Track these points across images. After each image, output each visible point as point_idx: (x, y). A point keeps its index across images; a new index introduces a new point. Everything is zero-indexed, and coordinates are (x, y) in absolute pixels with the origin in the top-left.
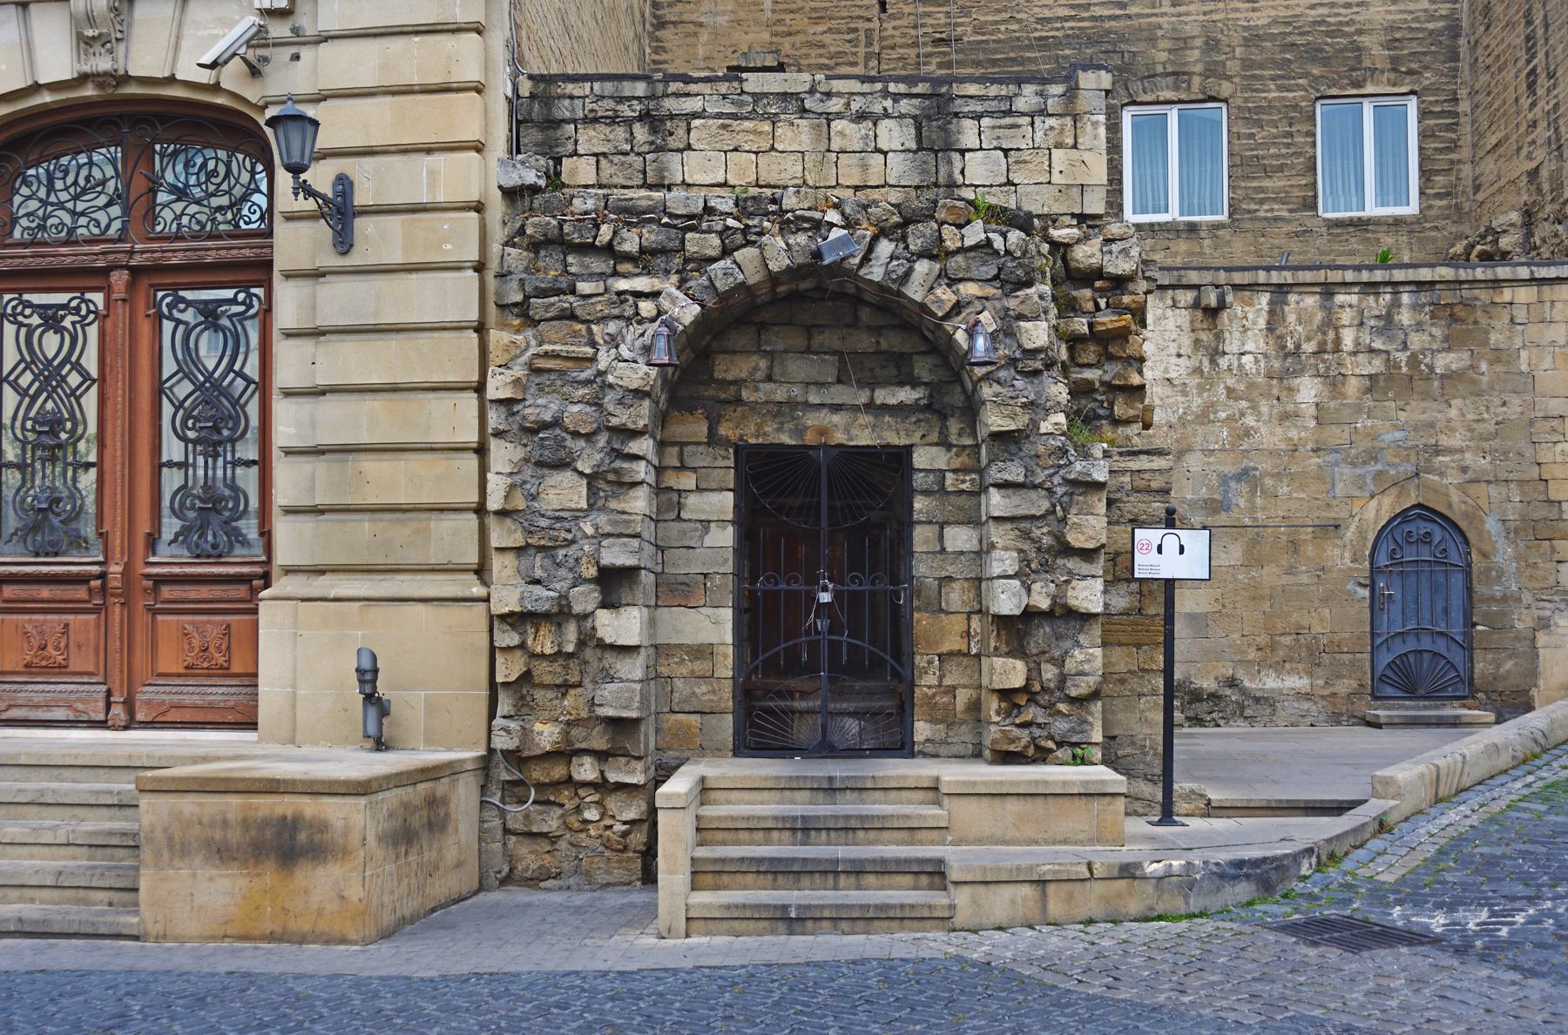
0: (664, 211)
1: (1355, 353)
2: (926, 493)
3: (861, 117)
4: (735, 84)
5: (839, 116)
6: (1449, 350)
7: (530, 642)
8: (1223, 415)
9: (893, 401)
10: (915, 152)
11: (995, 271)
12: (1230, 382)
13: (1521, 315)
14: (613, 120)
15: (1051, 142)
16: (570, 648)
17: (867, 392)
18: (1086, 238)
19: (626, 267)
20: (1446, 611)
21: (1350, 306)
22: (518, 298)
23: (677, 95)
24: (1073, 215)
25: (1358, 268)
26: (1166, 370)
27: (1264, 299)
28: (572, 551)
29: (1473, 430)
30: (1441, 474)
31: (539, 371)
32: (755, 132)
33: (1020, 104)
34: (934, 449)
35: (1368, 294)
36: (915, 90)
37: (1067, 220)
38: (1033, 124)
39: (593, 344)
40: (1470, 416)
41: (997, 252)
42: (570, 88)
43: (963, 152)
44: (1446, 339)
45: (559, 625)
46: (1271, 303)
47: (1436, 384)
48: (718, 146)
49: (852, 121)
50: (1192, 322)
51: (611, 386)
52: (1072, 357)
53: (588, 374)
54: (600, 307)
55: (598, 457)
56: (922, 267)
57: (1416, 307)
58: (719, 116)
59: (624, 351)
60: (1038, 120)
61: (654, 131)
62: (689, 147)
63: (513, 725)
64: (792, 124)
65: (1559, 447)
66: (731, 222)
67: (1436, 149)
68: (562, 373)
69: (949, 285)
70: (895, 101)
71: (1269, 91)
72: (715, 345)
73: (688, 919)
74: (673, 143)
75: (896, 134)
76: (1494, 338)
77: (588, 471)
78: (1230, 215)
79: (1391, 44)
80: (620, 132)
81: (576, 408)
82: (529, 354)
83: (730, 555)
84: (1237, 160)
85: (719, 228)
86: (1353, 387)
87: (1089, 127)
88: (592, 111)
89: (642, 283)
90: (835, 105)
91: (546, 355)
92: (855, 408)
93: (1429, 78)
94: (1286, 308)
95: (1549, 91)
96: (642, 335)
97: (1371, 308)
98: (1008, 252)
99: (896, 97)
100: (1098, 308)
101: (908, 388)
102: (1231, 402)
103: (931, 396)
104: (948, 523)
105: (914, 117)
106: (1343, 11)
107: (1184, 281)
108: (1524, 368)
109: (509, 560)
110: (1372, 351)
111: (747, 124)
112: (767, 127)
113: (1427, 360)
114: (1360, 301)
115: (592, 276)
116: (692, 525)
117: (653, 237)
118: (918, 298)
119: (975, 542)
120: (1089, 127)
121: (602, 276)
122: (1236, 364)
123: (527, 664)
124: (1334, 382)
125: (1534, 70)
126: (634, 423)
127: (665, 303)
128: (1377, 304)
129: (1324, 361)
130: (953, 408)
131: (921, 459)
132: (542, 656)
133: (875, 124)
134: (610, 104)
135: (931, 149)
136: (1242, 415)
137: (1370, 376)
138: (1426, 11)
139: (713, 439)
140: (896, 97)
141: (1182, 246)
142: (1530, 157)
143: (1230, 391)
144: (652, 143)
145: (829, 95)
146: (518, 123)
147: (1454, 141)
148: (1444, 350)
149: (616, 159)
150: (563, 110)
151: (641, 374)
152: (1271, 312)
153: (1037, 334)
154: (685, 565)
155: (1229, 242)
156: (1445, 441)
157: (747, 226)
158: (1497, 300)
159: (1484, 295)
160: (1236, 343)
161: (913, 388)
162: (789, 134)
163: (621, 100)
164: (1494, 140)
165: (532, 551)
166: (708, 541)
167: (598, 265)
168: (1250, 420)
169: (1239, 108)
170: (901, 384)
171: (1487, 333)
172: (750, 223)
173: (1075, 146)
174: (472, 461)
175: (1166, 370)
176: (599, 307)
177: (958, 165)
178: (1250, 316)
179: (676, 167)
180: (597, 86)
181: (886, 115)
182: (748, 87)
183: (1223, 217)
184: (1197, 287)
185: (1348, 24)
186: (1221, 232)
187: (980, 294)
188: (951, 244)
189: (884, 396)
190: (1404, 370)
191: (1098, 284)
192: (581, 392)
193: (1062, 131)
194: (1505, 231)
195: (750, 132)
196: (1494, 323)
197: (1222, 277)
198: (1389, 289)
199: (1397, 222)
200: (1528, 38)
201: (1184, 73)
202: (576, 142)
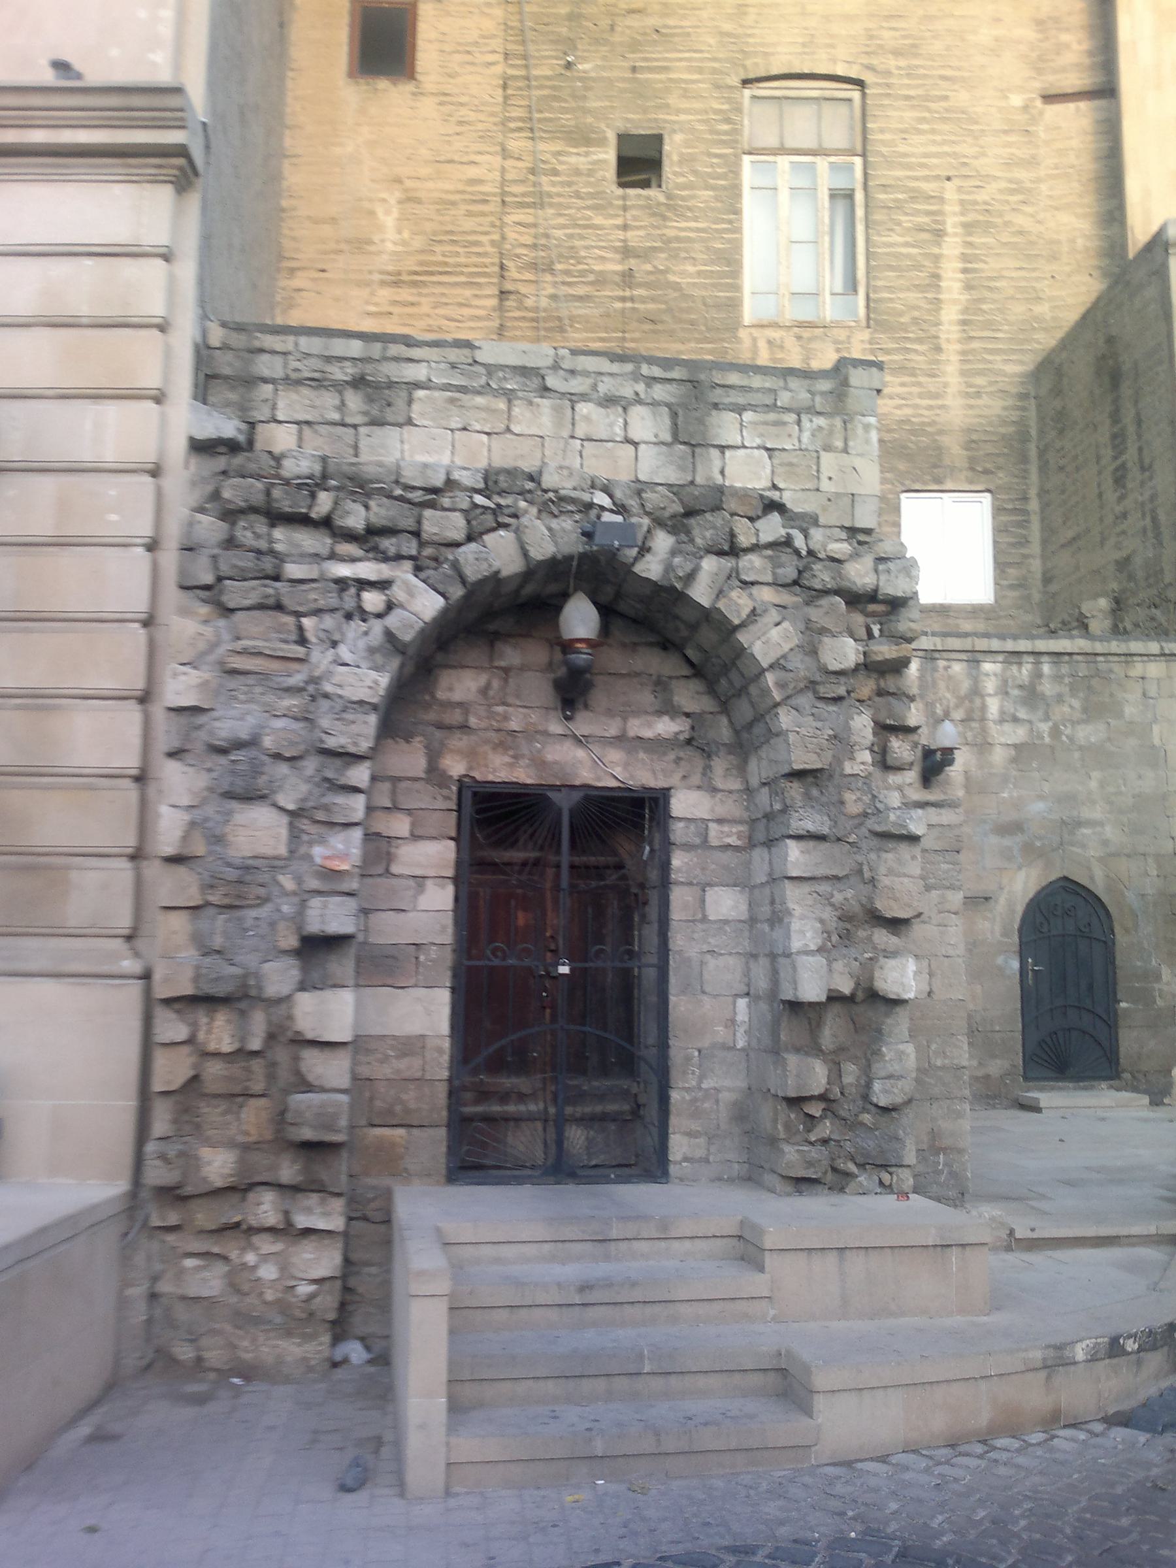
2: (688, 847)
3: (609, 401)
4: (466, 351)
5: (584, 397)
6: (1086, 721)
7: (201, 1036)
9: (648, 733)
11: (794, 575)
13: (1153, 691)
14: (318, 383)
15: (818, 445)
16: (255, 1044)
18: (856, 555)
20: (1090, 987)
22: (209, 579)
23: (396, 359)
24: (842, 527)
25: (1002, 637)
28: (264, 912)
29: (1111, 803)
30: (1084, 846)
31: (234, 672)
32: (487, 409)
35: (1011, 663)
36: (669, 375)
38: (799, 423)
39: (302, 641)
40: (1111, 789)
41: (797, 552)
42: (269, 341)
43: (722, 448)
44: (1085, 710)
45: (243, 1013)
47: (1077, 755)
48: (444, 423)
49: (600, 405)
51: (326, 696)
53: (297, 680)
54: (315, 596)
55: (304, 788)
56: (709, 564)
57: (1057, 678)
58: (447, 387)
59: (344, 652)
60: (804, 418)
61: (370, 400)
62: (410, 422)
63: (172, 1150)
64: (531, 403)
66: (479, 499)
68: (263, 676)
70: (648, 386)
73: (449, 1464)
77: (291, 807)
79: (969, 445)
80: (329, 399)
81: (280, 723)
82: (221, 650)
85: (465, 505)
86: (999, 756)
87: (860, 431)
88: (297, 370)
89: (368, 570)
90: (577, 385)
91: (245, 652)
95: (1142, 483)
97: (1014, 678)
98: (811, 553)
99: (651, 381)
100: (870, 635)
101: (666, 718)
104: (710, 885)
105: (668, 405)
106: (926, 413)
109: (179, 923)
111: (480, 400)
112: (502, 405)
113: (1068, 731)
114: (1004, 670)
116: (404, 882)
117: (383, 512)
118: (705, 602)
119: (744, 907)
121: (317, 557)
123: (195, 1066)
125: (1123, 467)
126: (355, 744)
127: (398, 593)
131: (686, 804)
132: (217, 1055)
133: (625, 409)
137: (1015, 746)
138: (999, 416)
139: (435, 775)
140: (651, 381)
142: (1118, 547)
149: (323, 429)
150: (266, 366)
154: (392, 930)
156: (1086, 813)
157: (499, 506)
159: (1118, 669)
161: (672, 719)
162: (528, 415)
163: (329, 359)
164: (1070, 534)
165: (211, 911)
167: (310, 541)
170: (660, 713)
172: (503, 502)
173: (845, 450)
174: (131, 793)
176: (313, 596)
177: (717, 464)
181: (639, 401)
182: (481, 356)
185: (929, 424)
187: (777, 601)
188: (744, 540)
189: (638, 727)
190: (1047, 740)
191: (872, 607)
193: (831, 433)
196: (1128, 696)
198: (1031, 659)
200: (1114, 437)
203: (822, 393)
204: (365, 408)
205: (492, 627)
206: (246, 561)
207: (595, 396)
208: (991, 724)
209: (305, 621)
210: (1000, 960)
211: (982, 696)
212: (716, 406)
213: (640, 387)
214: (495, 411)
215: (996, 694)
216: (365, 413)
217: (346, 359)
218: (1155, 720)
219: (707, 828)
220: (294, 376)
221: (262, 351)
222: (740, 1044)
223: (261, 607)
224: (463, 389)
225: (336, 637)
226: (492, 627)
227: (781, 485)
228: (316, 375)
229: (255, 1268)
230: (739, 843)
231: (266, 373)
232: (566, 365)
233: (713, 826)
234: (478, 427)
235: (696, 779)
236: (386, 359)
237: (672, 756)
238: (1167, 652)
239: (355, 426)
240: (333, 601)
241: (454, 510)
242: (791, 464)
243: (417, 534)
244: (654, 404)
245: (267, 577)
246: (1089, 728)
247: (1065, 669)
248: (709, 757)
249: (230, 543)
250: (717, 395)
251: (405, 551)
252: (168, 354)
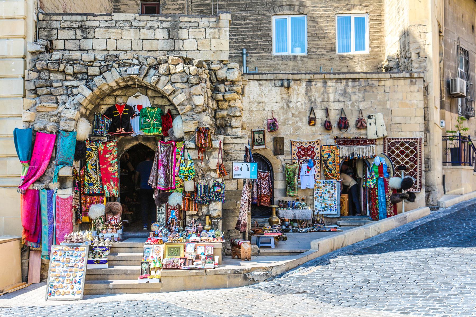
0: (81, 60)
1: (334, 102)
3: (150, 28)
4: (110, 17)
5: (143, 27)
8: (290, 123)
12: (293, 112)
13: (387, 90)
14: (70, 28)
15: (211, 37)
19: (69, 78)
21: (332, 86)
24: (218, 60)
26: (272, 107)
27: (304, 84)
36: (167, 20)
37: (216, 62)
39: (57, 103)
42: (55, 18)
43: (183, 40)
44: (364, 97)
46: (307, 85)
48: (104, 37)
49: (147, 29)
50: (281, 91)
52: (218, 106)
56: (163, 78)
58: (104, 27)
59: (67, 105)
61: (83, 32)
62: (94, 37)
65: (400, 133)
66: (103, 63)
67: (374, 32)
69: (171, 84)
70: (161, 23)
71: (320, 11)
72: (101, 102)
74: (89, 36)
75: (161, 34)
76: (379, 97)
78: (308, 53)
80: (72, 32)
84: (310, 34)
87: (223, 32)
89: (75, 83)
90: (142, 24)
93: (371, 8)
94: (312, 87)
96: (73, 100)
98: (190, 74)
100: (226, 91)
102: (293, 118)
107: (278, 78)
108: (388, 107)
110: (339, 101)
111: (113, 30)
112: (120, 31)
113: (357, 104)
115: (57, 81)
117: (77, 68)
120: (223, 32)
121: (61, 81)
122: (295, 105)
128: (341, 86)
129: (324, 104)
133: (155, 30)
134: (69, 23)
135: (173, 39)
136: (297, 122)
141: (291, 63)
143: (293, 114)
144: (82, 36)
147: (380, 29)
148: (363, 101)
151: (72, 113)
152: (307, 88)
153: (199, 101)
155: (307, 62)
157: (108, 65)
158: (380, 85)
160: (295, 98)
162: (127, 33)
163: (72, 22)
168: (299, 124)
169: (310, 17)
171: (377, 95)
172: (109, 63)
175: (272, 107)
176: (59, 91)
178: (300, 90)
179: (87, 44)
180: (64, 17)
181: (158, 28)
183: (305, 54)
184: (282, 80)
186: (304, 59)
188: (172, 72)
190: (350, 107)
191: (226, 83)
192: (53, 118)
194: (391, 61)
195: (114, 33)
196: (379, 92)
197: (290, 77)
198: (345, 81)
201: (293, 5)
204: (82, 34)
205: (115, 94)
206: (42, 82)
208: (331, 103)
209: (58, 97)
212: (181, 28)
213: (159, 24)
214: (118, 33)
216: (82, 36)
217: (76, 21)
218: (388, 100)
220: (62, 27)
223: (47, 94)
224: (109, 27)
225: (66, 101)
226: (115, 94)
227: (200, 49)
228: (69, 26)
231: (55, 26)
232: (138, 19)
234: (113, 38)
236: (87, 20)
238: (393, 77)
239: (79, 40)
240: (65, 92)
241: (96, 66)
242: (203, 43)
243: (87, 73)
245: (48, 86)
246: (365, 103)
247: (357, 83)
249: (39, 78)
250: (181, 25)
251: (84, 77)
252: (26, 26)
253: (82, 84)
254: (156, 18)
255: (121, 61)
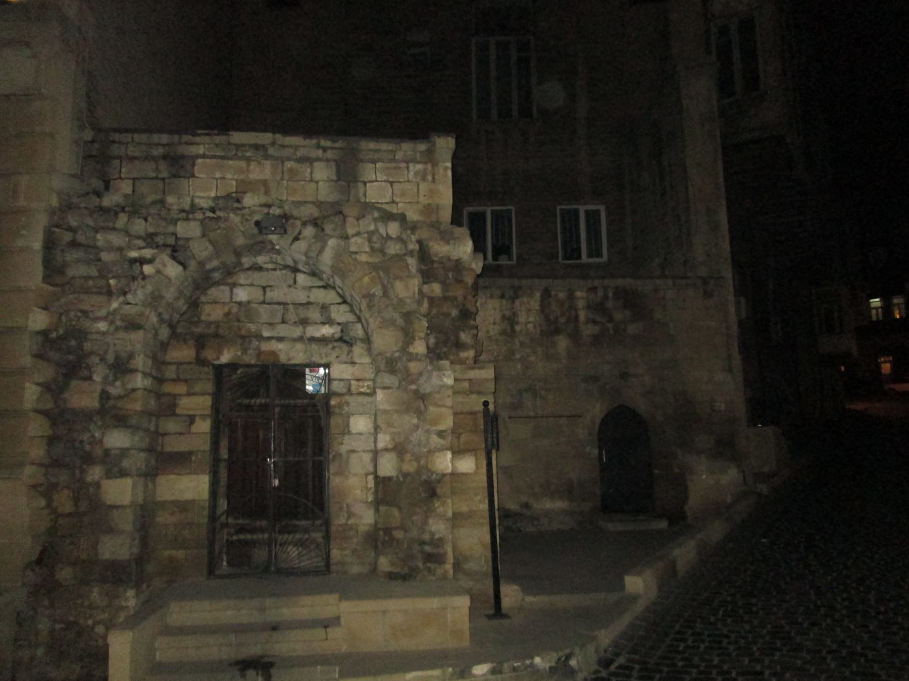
3: (301, 160)
5: (289, 159)
8: (518, 356)
9: (318, 334)
10: (336, 181)
12: (521, 338)
14: (148, 158)
17: (301, 328)
26: (488, 332)
33: (399, 155)
34: (344, 366)
38: (408, 168)
60: (411, 165)
64: (260, 163)
83: (209, 435)
87: (441, 171)
89: (147, 253)
90: (286, 153)
92: (295, 340)
101: (327, 326)
103: (342, 331)
105: (335, 161)
120: (441, 171)
124: (575, 336)
130: (356, 339)
145: (283, 146)
146: (302, 319)
152: (542, 301)
161: (330, 326)
162: (258, 169)
163: (149, 145)
166: (194, 429)
168: (533, 359)
175: (488, 332)
177: (361, 191)
181: (318, 159)
190: (611, 332)
199: (598, 266)
202: (120, 171)
203: (421, 152)
207: (294, 157)
210: (588, 449)
211: (576, 310)
215: (584, 308)
219: (350, 385)
221: (113, 142)
222: (370, 500)
229: (93, 628)
230: (368, 391)
233: (353, 382)
235: (344, 357)
237: (330, 346)
239: (163, 179)
244: (328, 160)
248: (351, 345)
253: (165, 257)
254: (314, 141)
255: (247, 211)
